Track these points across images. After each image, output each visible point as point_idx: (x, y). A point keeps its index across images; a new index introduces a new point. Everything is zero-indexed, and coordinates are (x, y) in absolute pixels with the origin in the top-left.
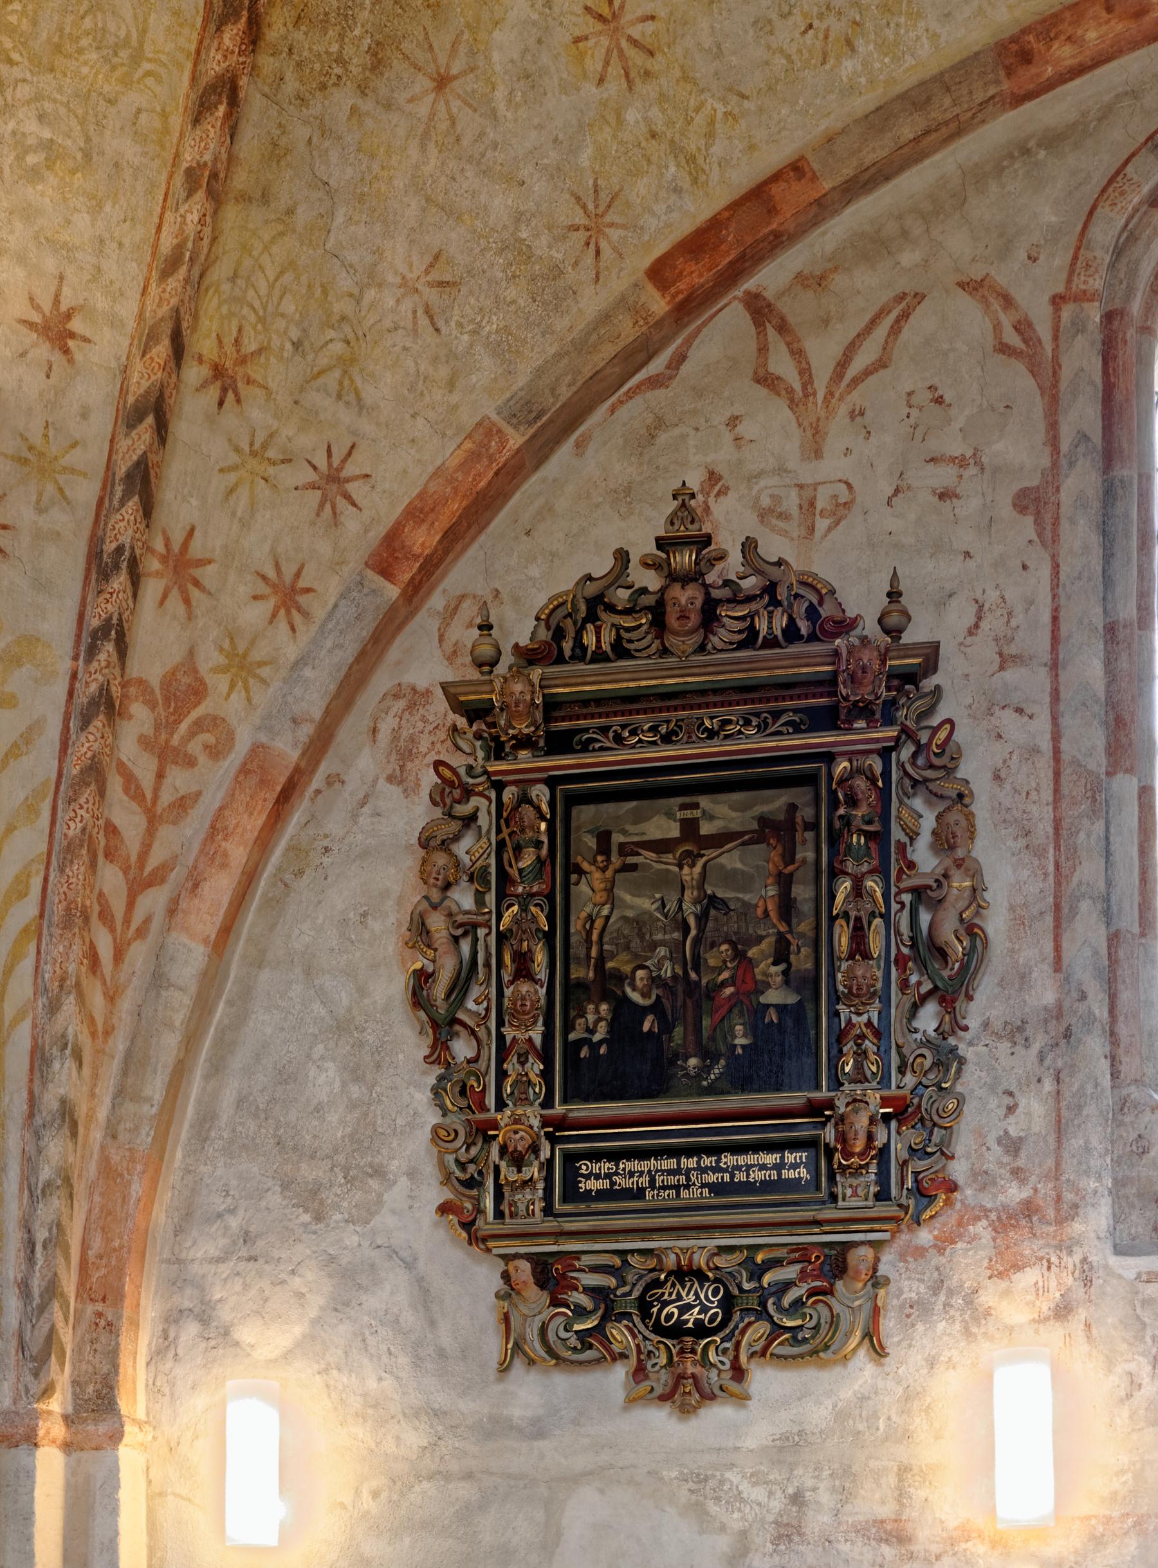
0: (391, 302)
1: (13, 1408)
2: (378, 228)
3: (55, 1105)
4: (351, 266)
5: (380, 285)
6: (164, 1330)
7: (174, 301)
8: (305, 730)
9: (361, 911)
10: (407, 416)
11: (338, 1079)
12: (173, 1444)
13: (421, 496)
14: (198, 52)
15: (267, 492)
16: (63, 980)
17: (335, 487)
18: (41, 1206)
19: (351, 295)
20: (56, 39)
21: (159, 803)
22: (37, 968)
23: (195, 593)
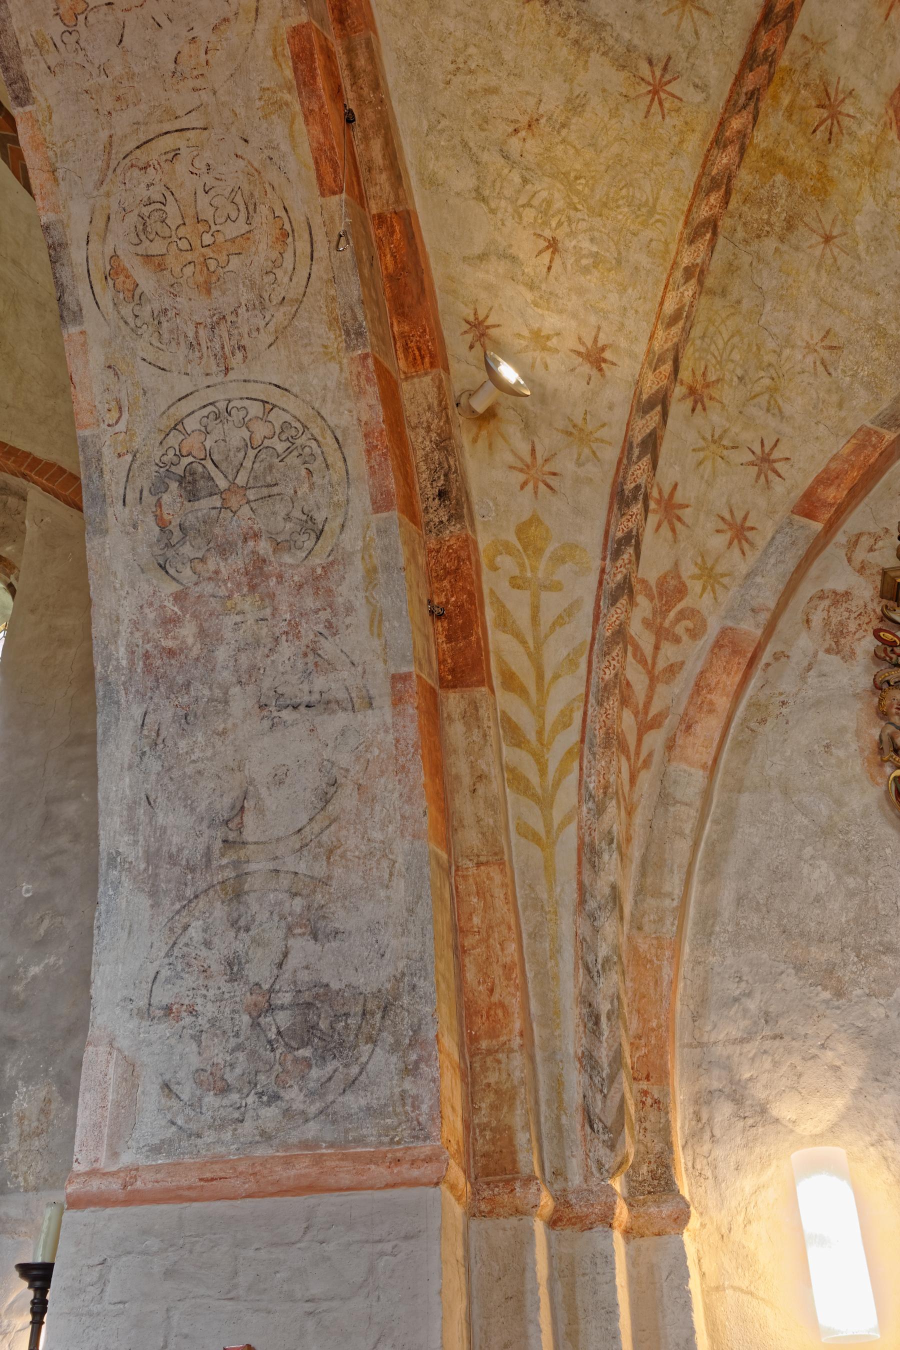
0: (800, 357)
1: (585, 1186)
2: (791, 314)
3: (607, 891)
4: (775, 335)
5: (793, 347)
6: (694, 1112)
7: (675, 340)
8: (763, 616)
9: (824, 743)
10: (813, 424)
11: (831, 874)
12: (724, 1230)
13: (826, 470)
14: (689, 210)
15: (723, 465)
16: (606, 788)
17: (767, 465)
18: (602, 980)
19: (775, 352)
20: (604, 200)
21: (656, 667)
22: (580, 781)
23: (678, 525)
